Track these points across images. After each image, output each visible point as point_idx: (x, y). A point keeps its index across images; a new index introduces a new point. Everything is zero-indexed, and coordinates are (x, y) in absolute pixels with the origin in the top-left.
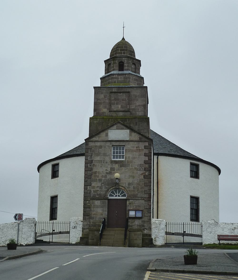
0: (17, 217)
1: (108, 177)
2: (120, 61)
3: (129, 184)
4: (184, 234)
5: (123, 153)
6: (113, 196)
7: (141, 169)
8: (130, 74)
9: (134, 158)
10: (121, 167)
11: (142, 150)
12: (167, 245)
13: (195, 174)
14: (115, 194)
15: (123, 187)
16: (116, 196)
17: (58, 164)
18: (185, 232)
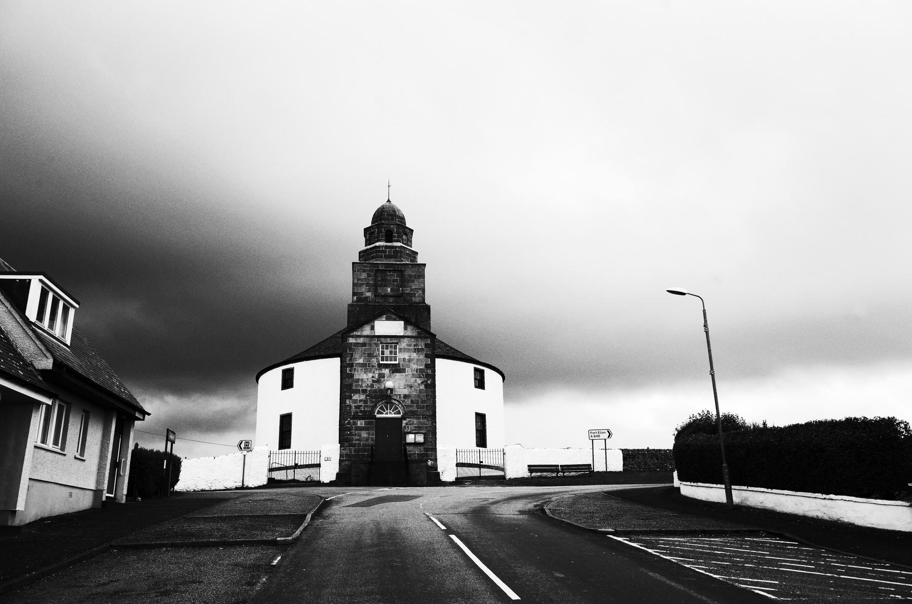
0: (243, 446)
1: (376, 386)
2: (388, 229)
3: (406, 396)
4: (480, 466)
6: (383, 414)
7: (421, 376)
8: (401, 246)
9: (410, 360)
10: (393, 372)
11: (422, 349)
12: (459, 482)
13: (480, 383)
14: (385, 411)
15: (398, 401)
16: (387, 414)
17: (292, 370)
18: (482, 462)
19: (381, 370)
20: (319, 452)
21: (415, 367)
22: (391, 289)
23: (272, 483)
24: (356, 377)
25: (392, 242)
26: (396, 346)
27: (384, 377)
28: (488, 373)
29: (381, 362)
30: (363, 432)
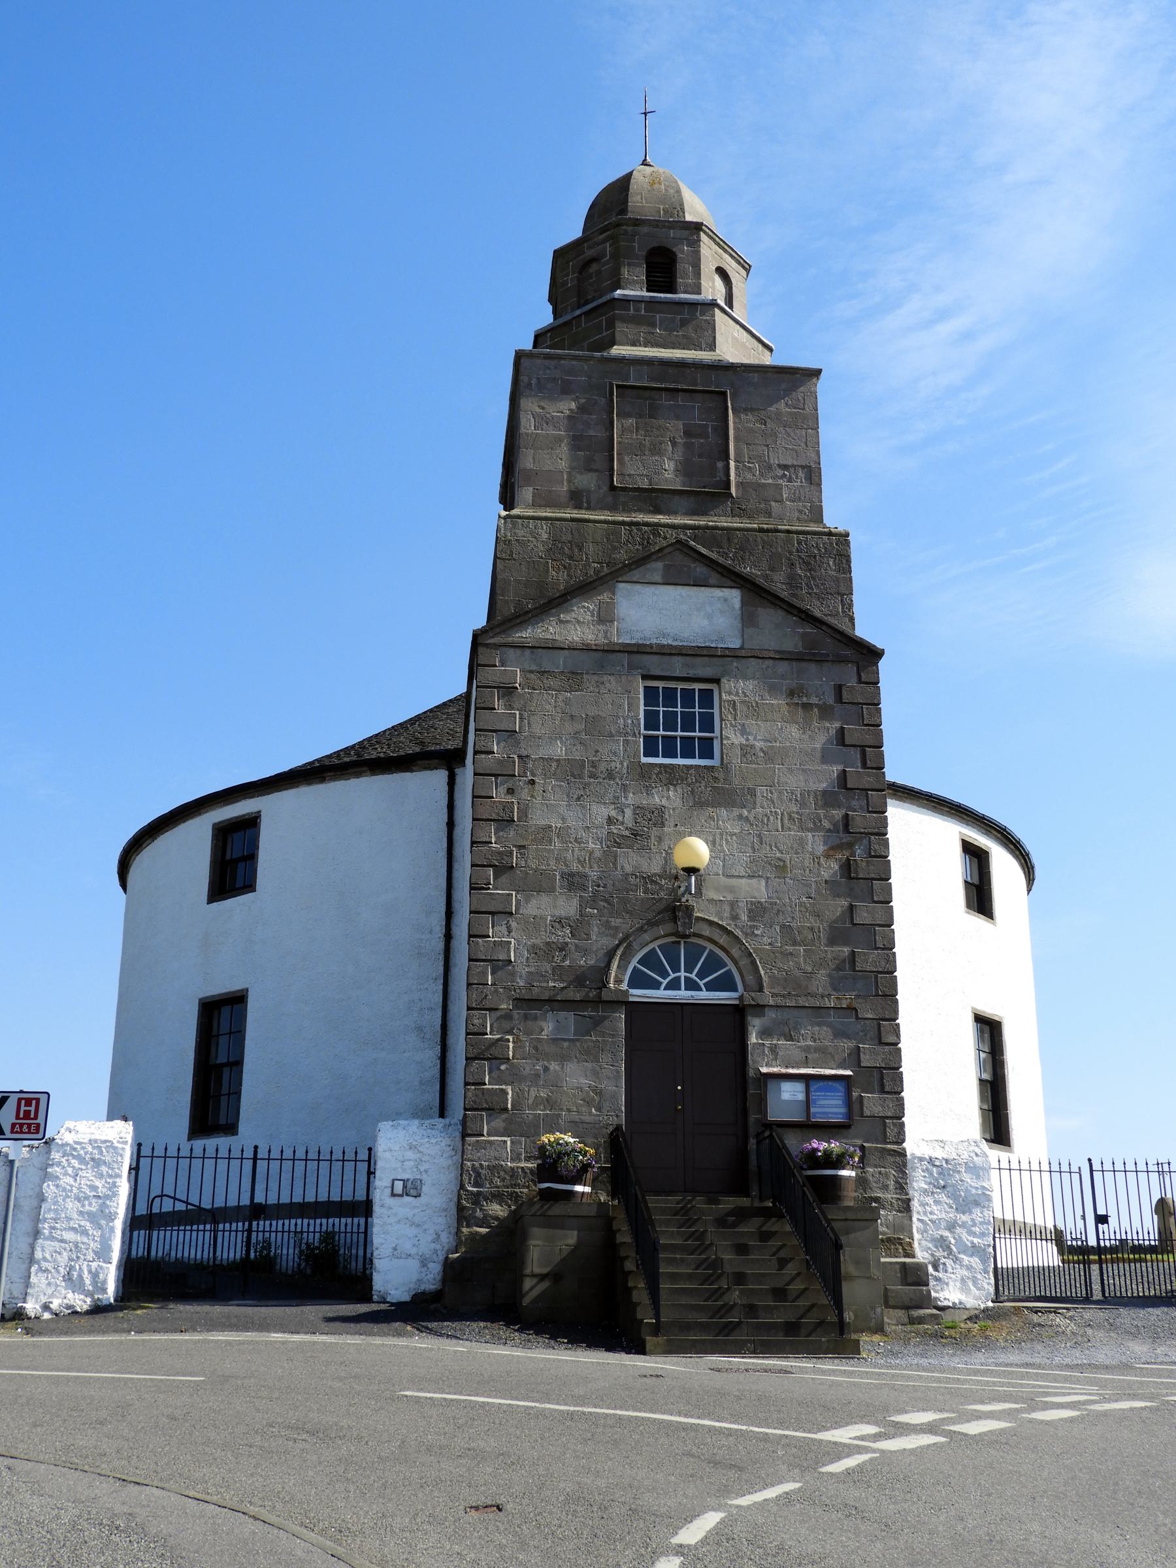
1: (630, 861)
5: (708, 724)
6: (656, 985)
10: (700, 804)
14: (701, 975)
16: (674, 985)
17: (251, 823)
19: (648, 790)
20: (363, 1155)
21: (794, 782)
24: (538, 818)
27: (663, 825)
29: (644, 760)
30: (571, 1067)
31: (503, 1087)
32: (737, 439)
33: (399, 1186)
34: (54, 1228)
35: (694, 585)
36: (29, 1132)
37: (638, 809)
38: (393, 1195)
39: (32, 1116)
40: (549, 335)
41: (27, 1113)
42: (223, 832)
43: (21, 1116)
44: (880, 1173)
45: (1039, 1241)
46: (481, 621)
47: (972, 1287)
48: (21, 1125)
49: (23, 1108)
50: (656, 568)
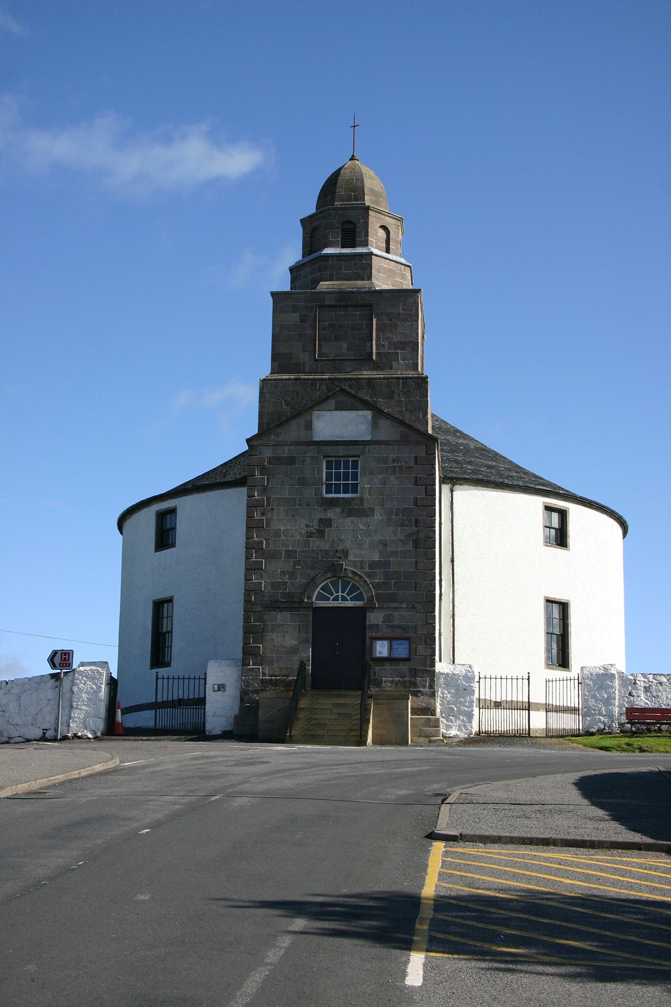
1: (316, 544)
5: (355, 477)
6: (328, 599)
16: (336, 599)
17: (173, 511)
19: (325, 510)
22: (348, 344)
23: (547, 736)
24: (275, 526)
25: (354, 247)
26: (357, 461)
28: (575, 511)
31: (259, 645)
32: (377, 330)
33: (216, 686)
34: (78, 705)
35: (349, 410)
36: (66, 666)
37: (321, 520)
38: (214, 691)
39: (67, 660)
40: (295, 269)
41: (65, 659)
42: (162, 516)
43: (63, 660)
44: (423, 680)
45: (502, 710)
46: (254, 430)
47: (463, 729)
48: (63, 664)
49: (63, 657)
50: (332, 402)
